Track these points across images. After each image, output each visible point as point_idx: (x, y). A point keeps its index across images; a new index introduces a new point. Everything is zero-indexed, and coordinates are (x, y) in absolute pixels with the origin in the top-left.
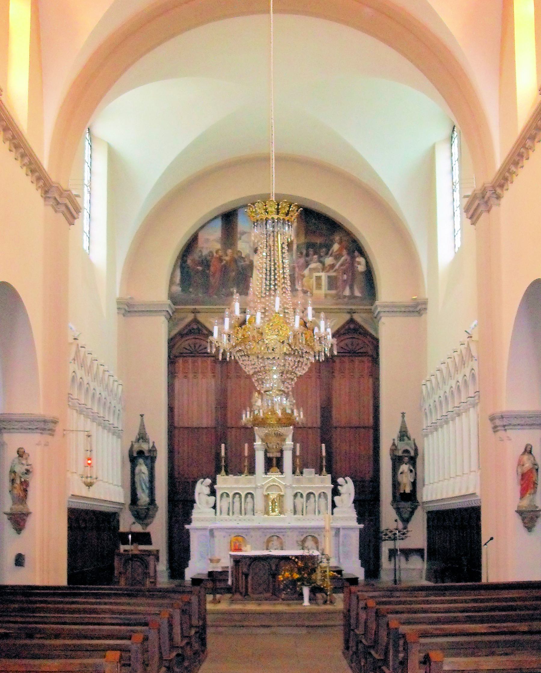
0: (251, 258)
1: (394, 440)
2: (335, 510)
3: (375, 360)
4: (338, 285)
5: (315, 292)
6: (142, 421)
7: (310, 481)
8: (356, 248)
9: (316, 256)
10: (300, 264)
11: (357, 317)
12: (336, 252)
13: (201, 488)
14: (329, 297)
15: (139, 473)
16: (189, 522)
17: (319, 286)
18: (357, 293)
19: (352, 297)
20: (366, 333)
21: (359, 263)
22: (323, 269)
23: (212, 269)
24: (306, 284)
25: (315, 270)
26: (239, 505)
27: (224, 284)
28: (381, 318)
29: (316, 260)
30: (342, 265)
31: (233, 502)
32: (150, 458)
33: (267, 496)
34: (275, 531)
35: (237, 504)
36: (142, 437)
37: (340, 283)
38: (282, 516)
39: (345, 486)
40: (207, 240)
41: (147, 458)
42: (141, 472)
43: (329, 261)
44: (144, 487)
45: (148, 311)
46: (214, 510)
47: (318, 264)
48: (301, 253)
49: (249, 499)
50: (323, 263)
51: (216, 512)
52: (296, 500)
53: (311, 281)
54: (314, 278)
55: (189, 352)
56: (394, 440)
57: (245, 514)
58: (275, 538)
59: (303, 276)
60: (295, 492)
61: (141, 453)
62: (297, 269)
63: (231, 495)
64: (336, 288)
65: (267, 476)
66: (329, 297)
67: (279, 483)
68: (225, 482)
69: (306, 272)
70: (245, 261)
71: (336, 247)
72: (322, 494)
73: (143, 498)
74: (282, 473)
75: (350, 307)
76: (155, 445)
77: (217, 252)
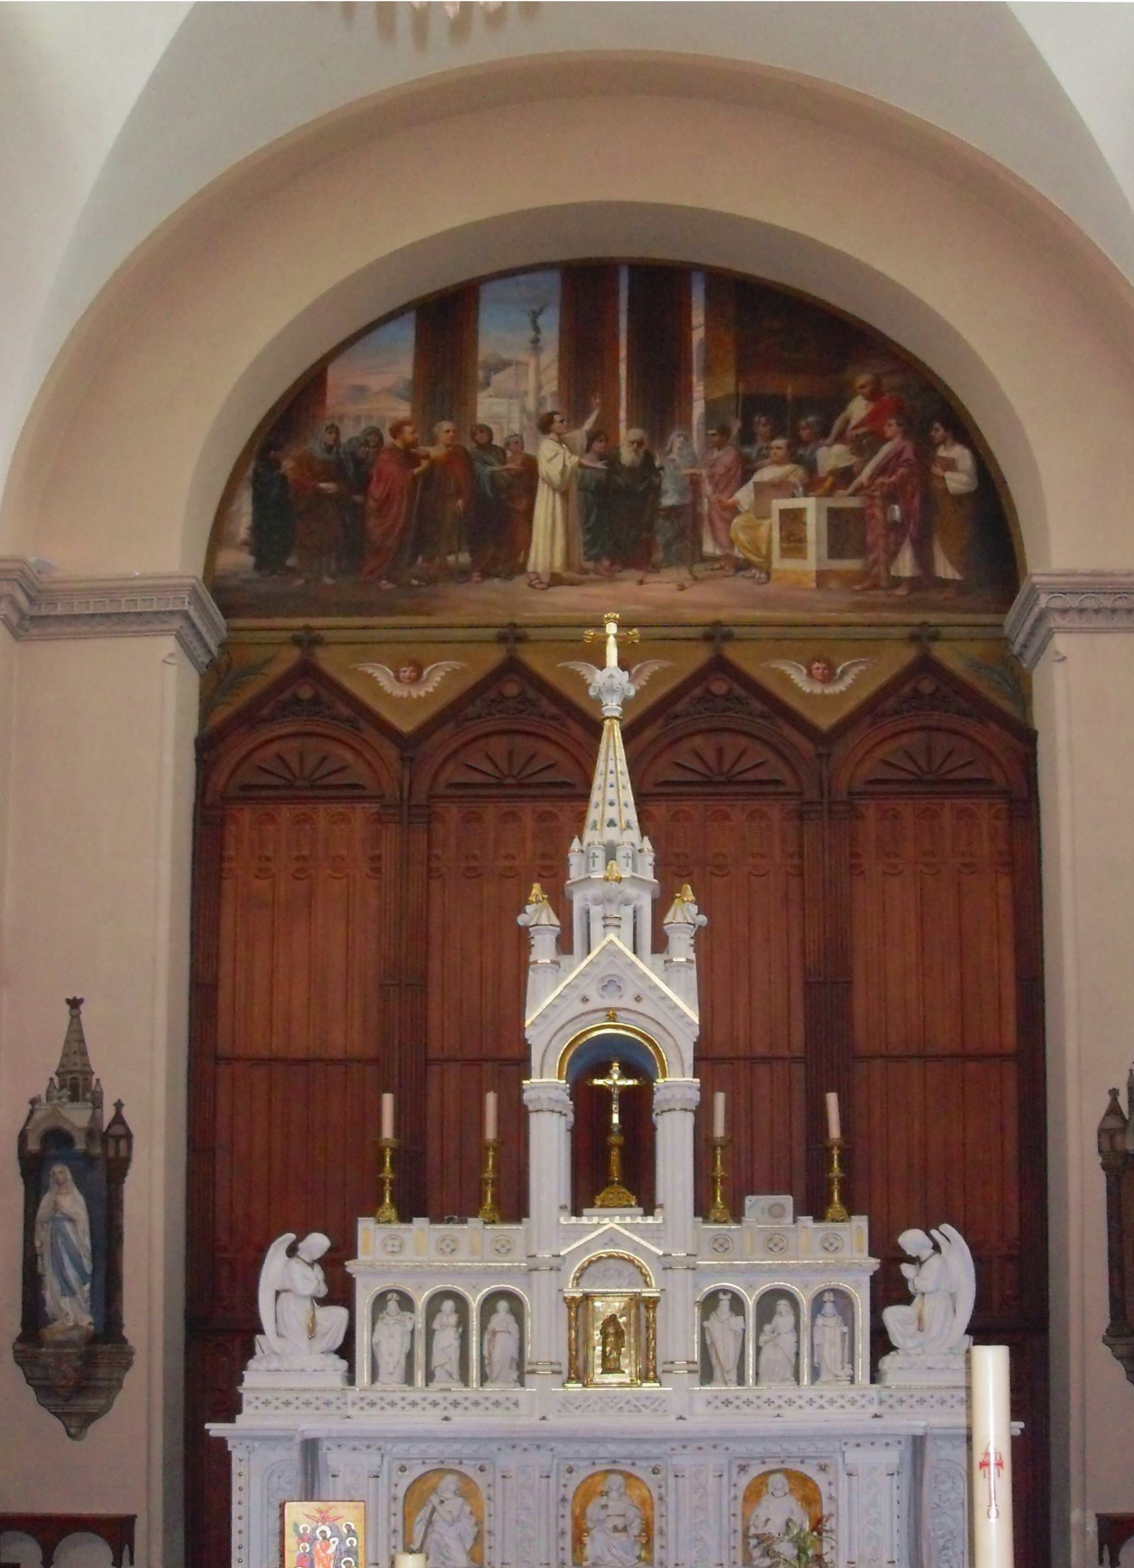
0: (528, 450)
1: (1114, 1093)
2: (888, 1362)
3: (1022, 806)
4: (870, 539)
5: (779, 564)
6: (75, 1019)
7: (774, 1245)
8: (931, 408)
9: (780, 442)
10: (720, 469)
11: (941, 652)
12: (856, 427)
13: (287, 1276)
14: (834, 584)
15: (53, 1219)
16: (230, 1409)
17: (793, 542)
18: (945, 569)
19: (925, 580)
20: (988, 712)
21: (951, 465)
22: (809, 488)
23: (377, 490)
24: (742, 537)
25: (780, 487)
26: (456, 1343)
27: (422, 537)
28: (1050, 634)
29: (780, 453)
30: (883, 470)
31: (430, 1334)
32: (102, 1162)
33: (580, 1306)
34: (612, 1449)
35: (447, 1339)
36: (75, 1081)
37: (874, 534)
38: (649, 1387)
39: (934, 1264)
40: (361, 391)
41: (89, 1159)
42: (59, 1217)
43: (832, 456)
44: (71, 1273)
45: (113, 613)
46: (343, 1364)
47: (788, 468)
48: (724, 431)
49: (502, 1316)
50: (811, 467)
51: (351, 1369)
52: (713, 1324)
53: (763, 531)
54: (775, 517)
55: (283, 782)
56: (1114, 1093)
57: (484, 1378)
58: (616, 1480)
59: (734, 510)
60: (707, 1289)
61: (57, 1139)
62: (707, 488)
63: (421, 1301)
64: (862, 550)
65: (584, 1220)
66: (834, 584)
67: (637, 1248)
68: (395, 1251)
69: (744, 496)
70: (503, 461)
71: (859, 409)
72: (829, 1297)
73: (71, 1312)
74: (649, 1205)
75: (916, 618)
76: (125, 1112)
77: (396, 430)
